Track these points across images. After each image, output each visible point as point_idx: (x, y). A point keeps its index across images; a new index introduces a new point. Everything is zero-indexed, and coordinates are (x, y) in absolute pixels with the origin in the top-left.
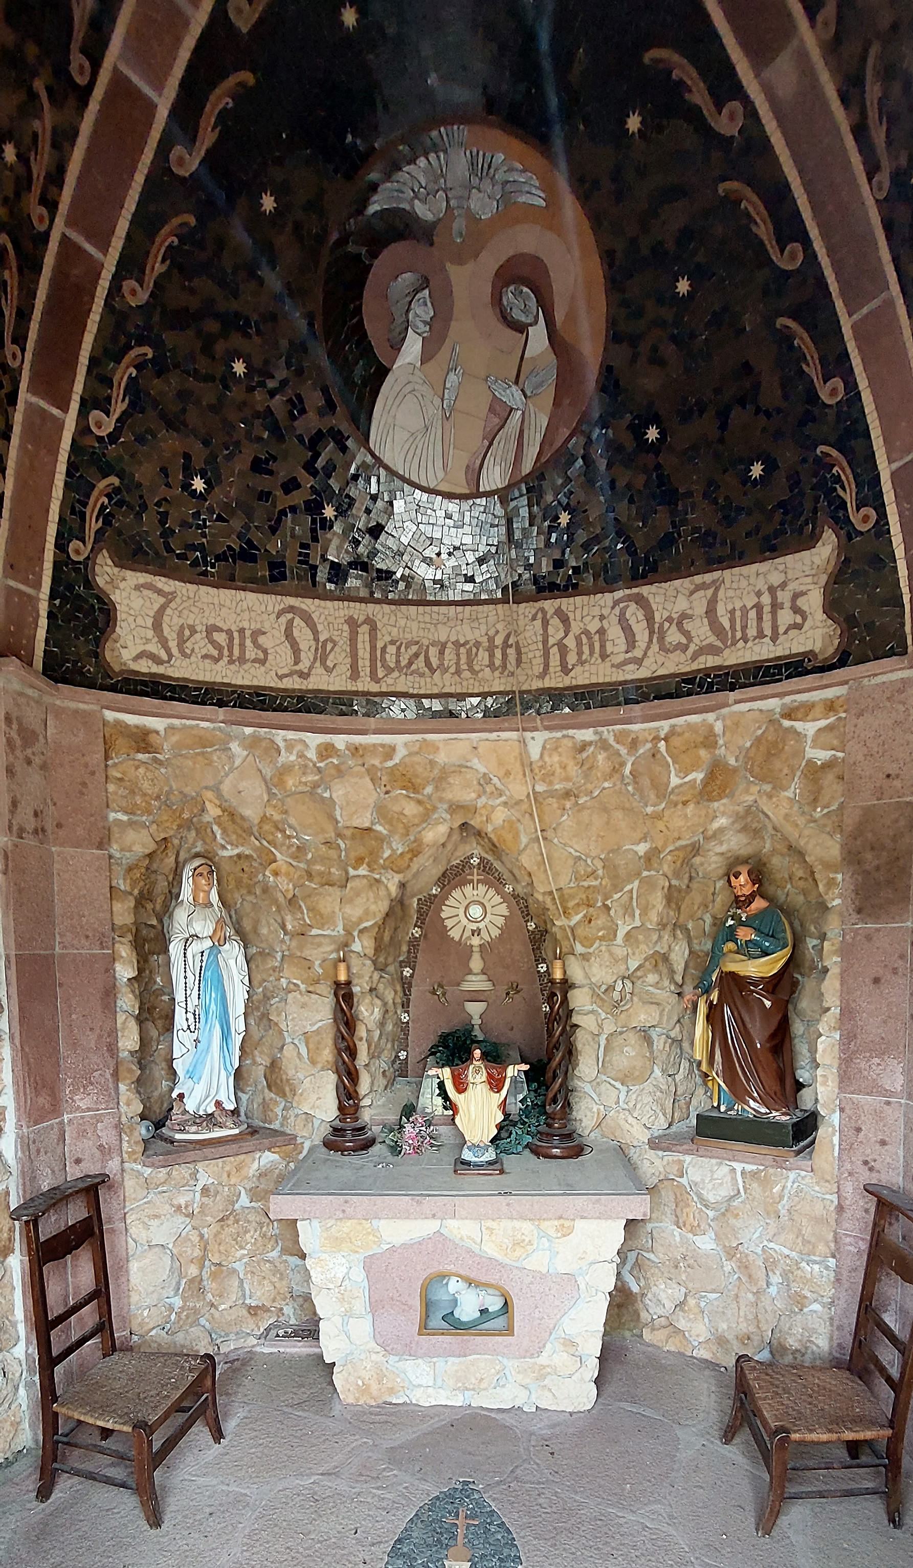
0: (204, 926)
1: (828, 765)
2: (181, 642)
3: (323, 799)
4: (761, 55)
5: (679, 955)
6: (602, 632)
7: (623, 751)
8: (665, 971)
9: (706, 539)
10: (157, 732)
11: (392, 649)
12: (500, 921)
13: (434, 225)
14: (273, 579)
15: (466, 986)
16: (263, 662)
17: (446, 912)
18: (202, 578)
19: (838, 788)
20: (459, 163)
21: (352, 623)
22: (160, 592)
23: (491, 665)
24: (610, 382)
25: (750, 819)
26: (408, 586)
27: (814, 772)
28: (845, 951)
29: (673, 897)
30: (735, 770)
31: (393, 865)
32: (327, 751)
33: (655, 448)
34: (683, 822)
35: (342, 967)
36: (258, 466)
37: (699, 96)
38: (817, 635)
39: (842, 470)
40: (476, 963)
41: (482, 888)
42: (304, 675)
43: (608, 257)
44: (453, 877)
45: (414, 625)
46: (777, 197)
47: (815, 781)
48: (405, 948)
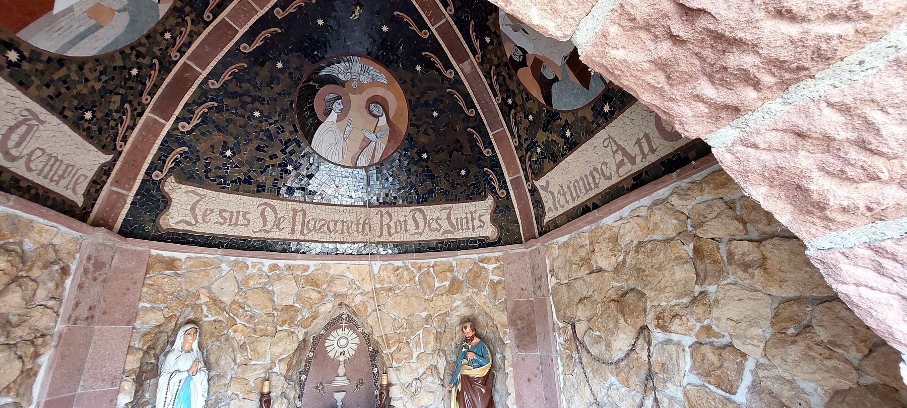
0: (185, 363)
1: (499, 282)
2: (205, 215)
3: (269, 291)
4: (460, 61)
5: (442, 364)
6: (405, 221)
7: (415, 271)
8: (436, 374)
9: (446, 192)
10: (180, 260)
11: (312, 222)
12: (355, 347)
13: (346, 82)
14: (258, 191)
15: (335, 384)
16: (247, 226)
17: (328, 343)
18: (223, 189)
19: (504, 292)
20: (357, 67)
21: (295, 211)
22: (198, 194)
23: (357, 231)
24: (409, 137)
25: (469, 303)
26: (322, 198)
27: (494, 285)
28: (514, 365)
29: (438, 337)
30: (462, 282)
31: (303, 325)
32: (274, 267)
33: (426, 160)
34: (442, 303)
35: (267, 383)
36: (258, 148)
37: (439, 65)
38: (489, 231)
39: (492, 176)
40: (341, 370)
41: (347, 330)
42: (266, 231)
43: (409, 102)
44: (333, 325)
45: (324, 213)
46: (466, 96)
47: (494, 289)
48: (303, 364)
